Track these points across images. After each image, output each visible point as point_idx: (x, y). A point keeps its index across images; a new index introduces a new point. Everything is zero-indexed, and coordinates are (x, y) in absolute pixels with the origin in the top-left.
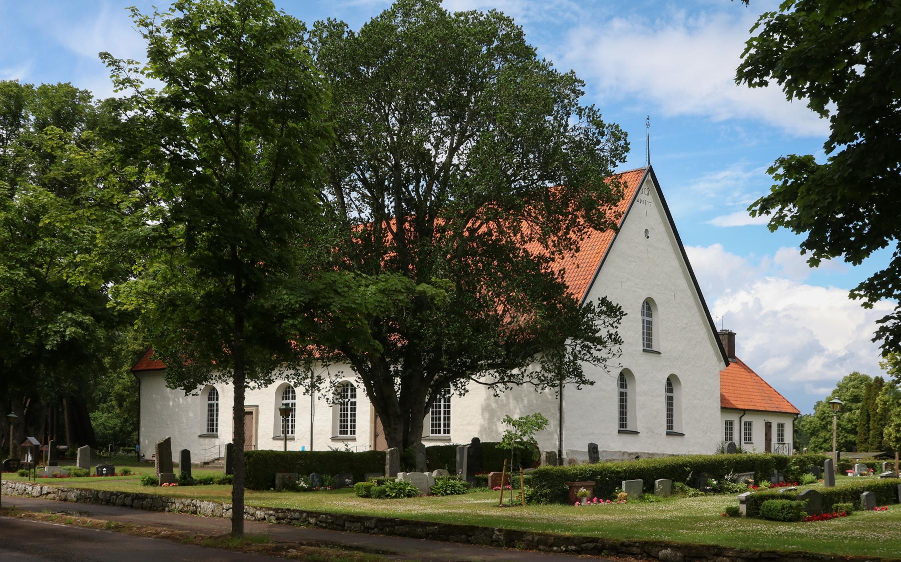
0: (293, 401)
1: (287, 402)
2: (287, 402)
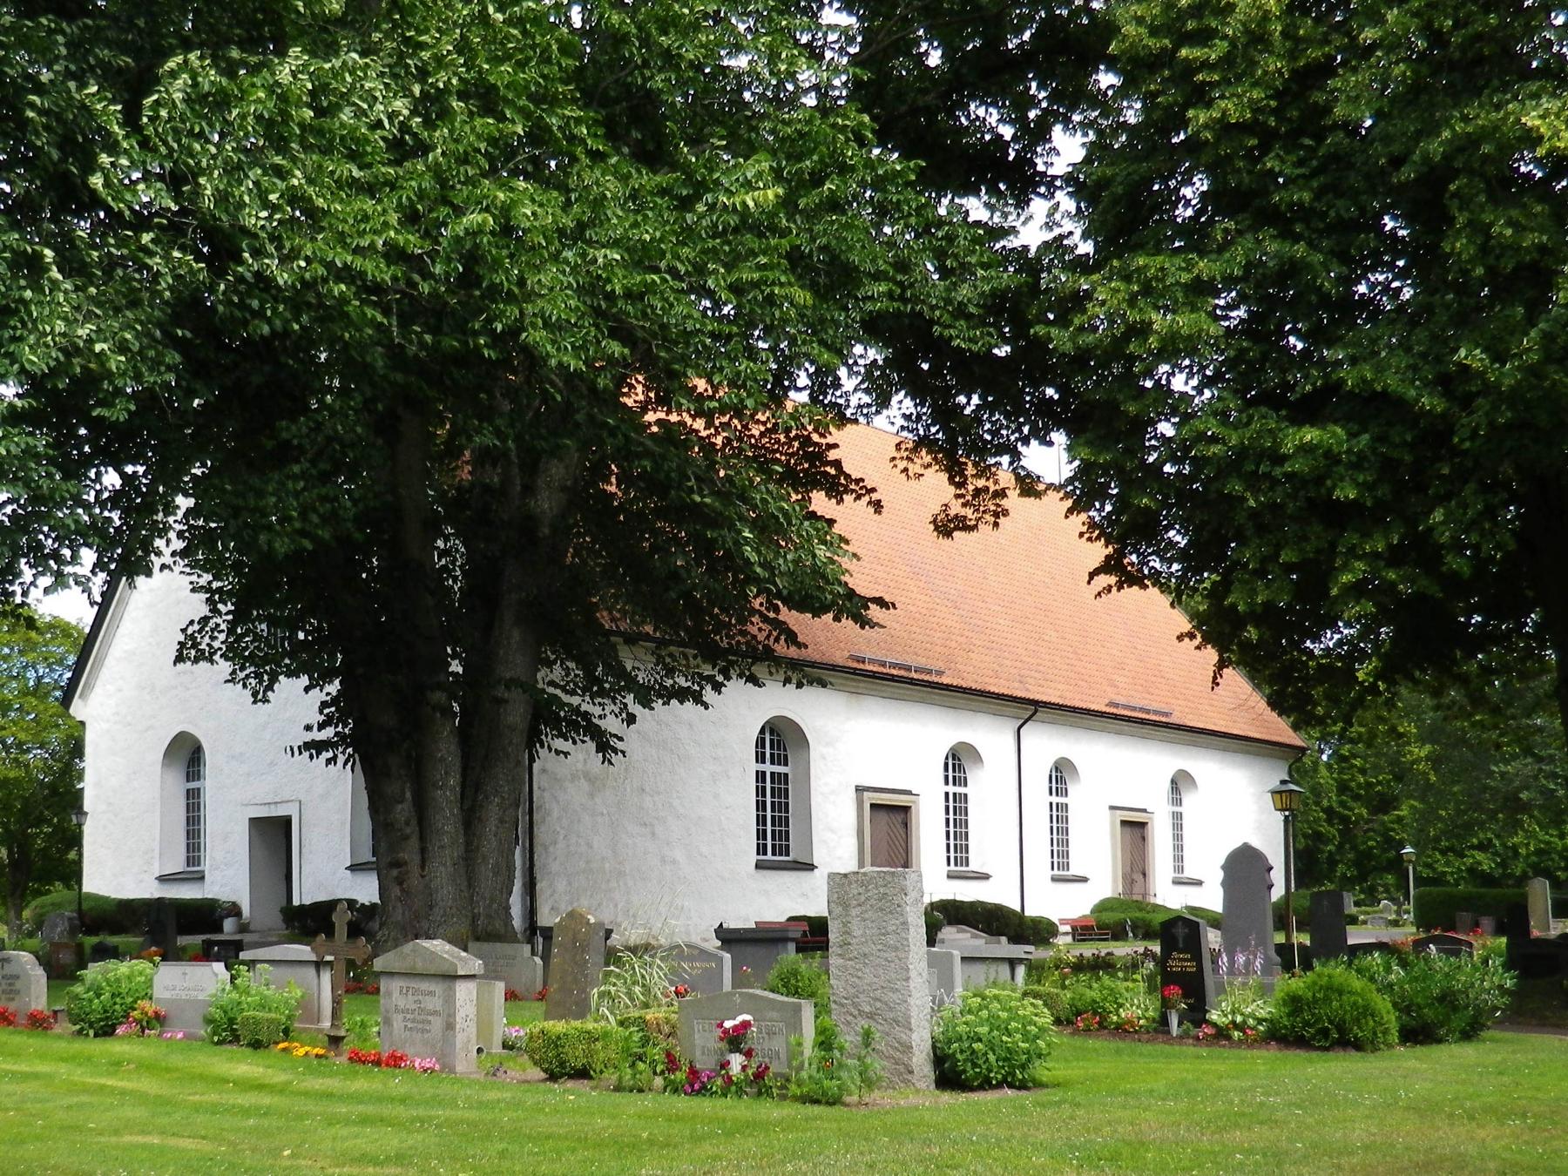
0: (761, 767)
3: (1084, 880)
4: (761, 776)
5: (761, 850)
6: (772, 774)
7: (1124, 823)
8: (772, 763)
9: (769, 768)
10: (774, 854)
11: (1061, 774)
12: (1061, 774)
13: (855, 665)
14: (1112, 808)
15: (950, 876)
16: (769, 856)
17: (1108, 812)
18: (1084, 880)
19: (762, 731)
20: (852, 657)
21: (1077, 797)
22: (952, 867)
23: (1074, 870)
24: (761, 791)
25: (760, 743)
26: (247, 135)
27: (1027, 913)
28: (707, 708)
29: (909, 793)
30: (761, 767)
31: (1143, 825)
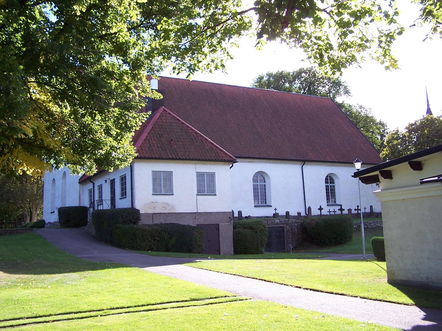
0: (327, 184)
2: (331, 185)
6: (260, 185)
30: (327, 184)
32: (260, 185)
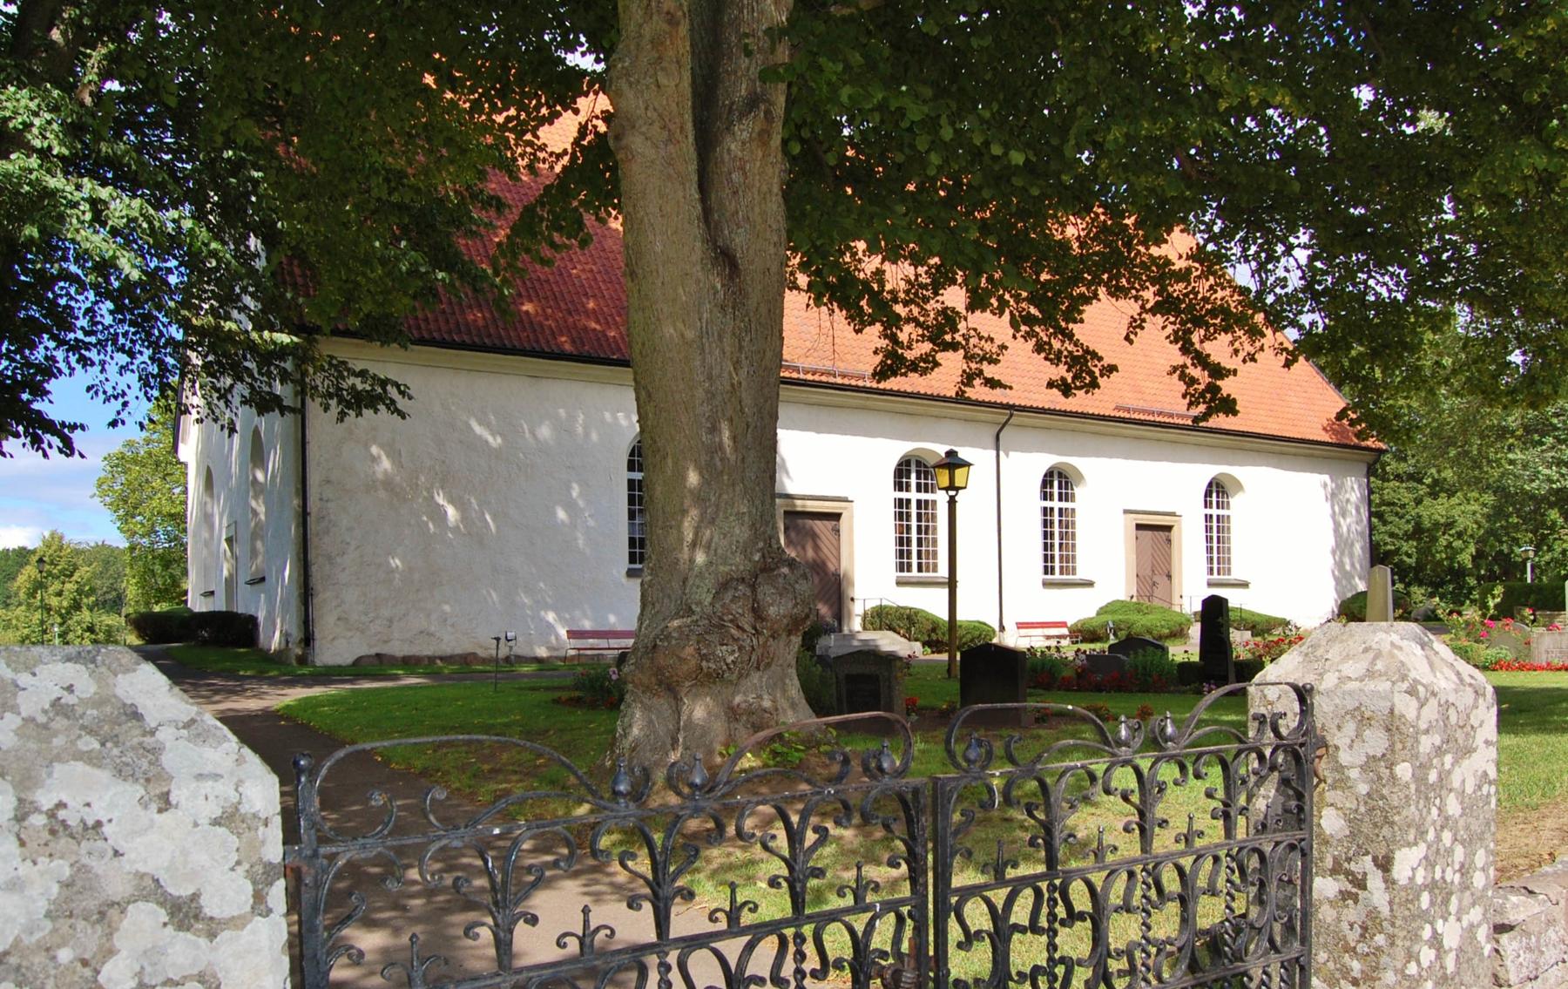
0: (1209, 511)
1: (923, 496)
3: (1090, 584)
4: (1208, 518)
5: (1048, 570)
6: (919, 502)
7: (1139, 527)
8: (1060, 499)
9: (1214, 512)
10: (1061, 573)
11: (1058, 482)
12: (1058, 482)
13: (1122, 414)
14: (1126, 512)
15: (900, 583)
16: (1057, 576)
17: (1122, 516)
18: (1090, 584)
19: (1210, 485)
20: (1118, 408)
21: (1084, 501)
22: (1215, 576)
23: (1081, 575)
24: (1208, 529)
25: (1208, 494)
26: (1281, 130)
27: (962, 615)
28: (404, 418)
29: (1173, 514)
30: (1209, 511)
31: (1169, 528)
32: (919, 502)
